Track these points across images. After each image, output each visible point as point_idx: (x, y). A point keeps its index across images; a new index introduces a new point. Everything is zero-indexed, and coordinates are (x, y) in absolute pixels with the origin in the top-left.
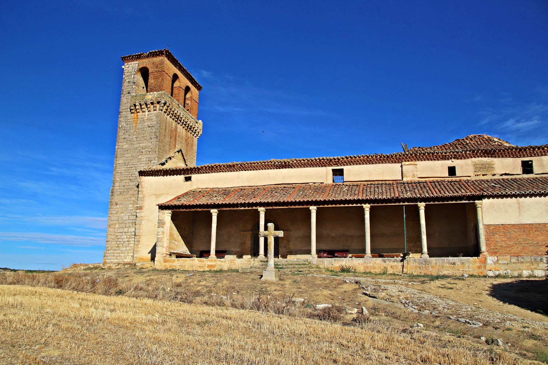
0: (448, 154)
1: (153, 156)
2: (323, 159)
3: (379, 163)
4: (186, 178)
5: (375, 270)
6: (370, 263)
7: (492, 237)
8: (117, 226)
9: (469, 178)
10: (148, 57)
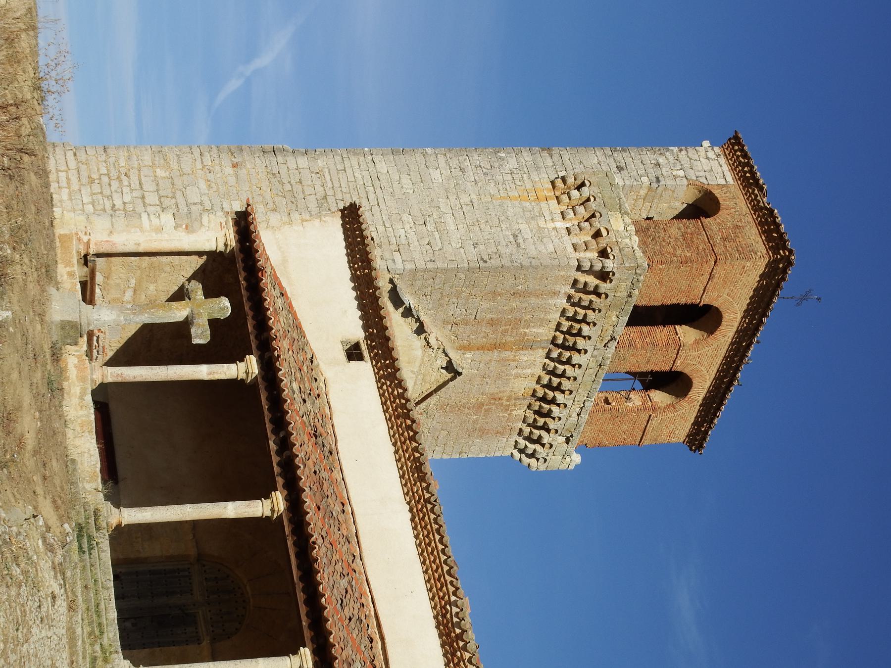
1: (417, 255)
4: (357, 346)
8: (160, 173)
10: (757, 208)
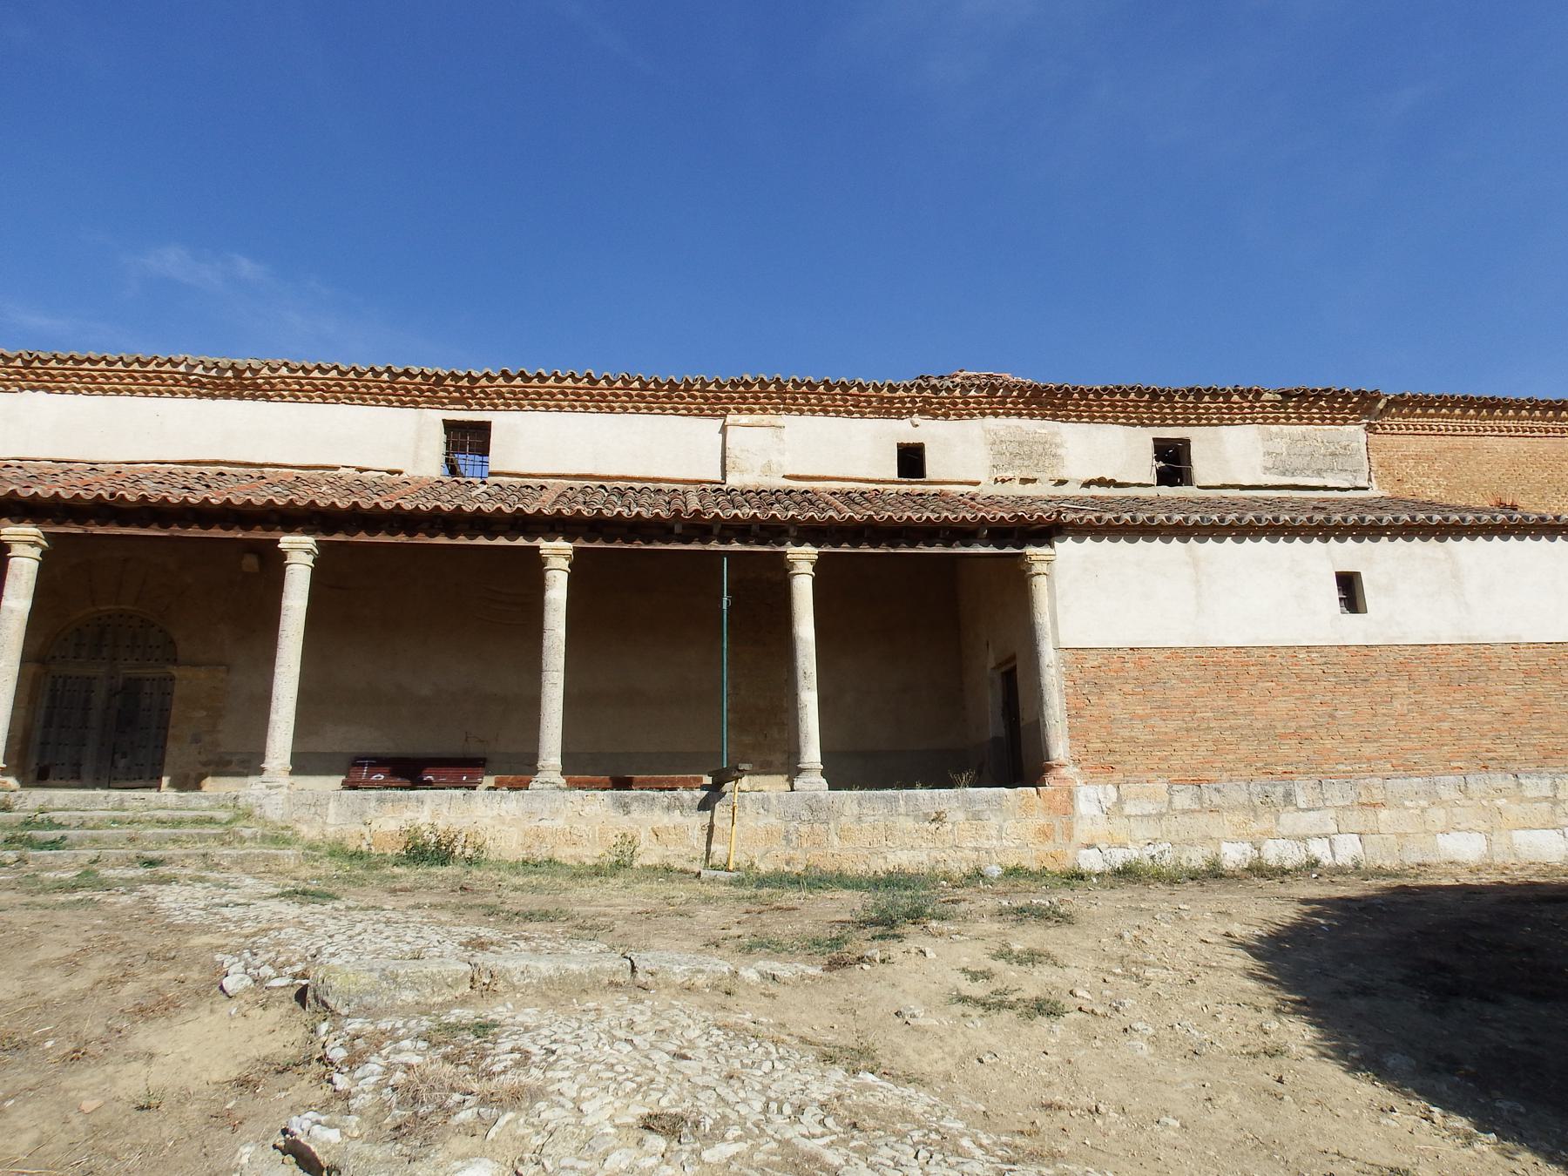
0: (901, 393)
2: (406, 373)
3: (638, 410)
5: (579, 850)
6: (556, 812)
7: (1094, 699)
9: (973, 489)
